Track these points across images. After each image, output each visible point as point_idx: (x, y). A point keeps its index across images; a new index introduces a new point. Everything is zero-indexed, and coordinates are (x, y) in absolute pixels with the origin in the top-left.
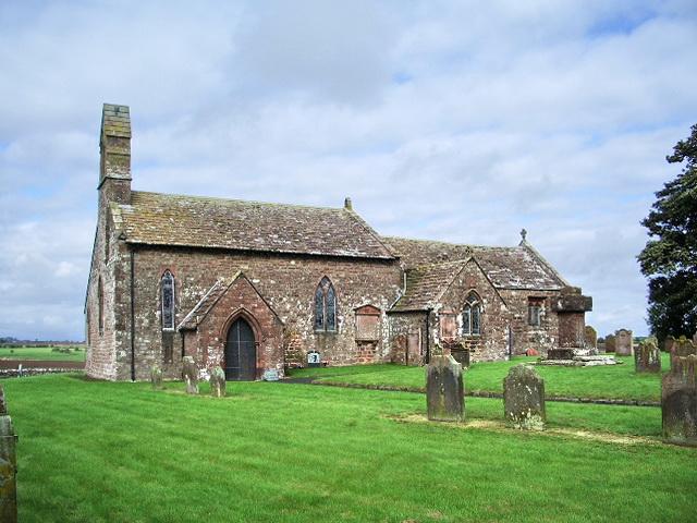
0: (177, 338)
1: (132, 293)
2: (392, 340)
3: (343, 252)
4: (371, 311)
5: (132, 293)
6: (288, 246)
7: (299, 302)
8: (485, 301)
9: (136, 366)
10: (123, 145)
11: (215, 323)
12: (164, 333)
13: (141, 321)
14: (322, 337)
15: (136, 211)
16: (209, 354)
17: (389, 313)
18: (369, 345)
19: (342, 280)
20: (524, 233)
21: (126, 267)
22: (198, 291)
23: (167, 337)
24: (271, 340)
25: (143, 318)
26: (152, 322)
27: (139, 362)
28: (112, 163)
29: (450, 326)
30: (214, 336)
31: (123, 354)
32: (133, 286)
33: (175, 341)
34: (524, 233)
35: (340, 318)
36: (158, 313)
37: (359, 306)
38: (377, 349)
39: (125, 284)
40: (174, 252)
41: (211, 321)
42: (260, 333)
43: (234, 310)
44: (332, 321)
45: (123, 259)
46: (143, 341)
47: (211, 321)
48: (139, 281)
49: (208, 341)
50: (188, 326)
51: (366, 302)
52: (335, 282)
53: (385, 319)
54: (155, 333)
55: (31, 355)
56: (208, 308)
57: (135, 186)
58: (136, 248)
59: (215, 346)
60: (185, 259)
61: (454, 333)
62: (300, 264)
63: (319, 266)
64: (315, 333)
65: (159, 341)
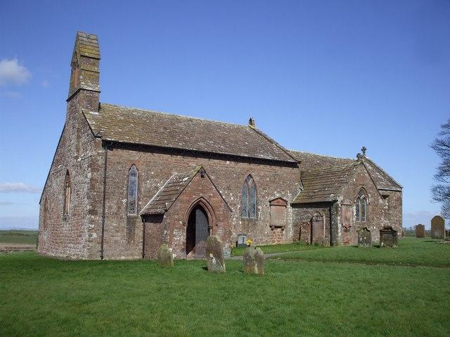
0: (139, 223)
1: (105, 183)
2: (295, 225)
3: (262, 156)
4: (280, 202)
5: (105, 183)
6: (222, 149)
7: (231, 194)
8: (370, 195)
9: (104, 246)
10: (94, 64)
11: (181, 209)
12: (129, 218)
13: (110, 207)
14: (247, 223)
15: (103, 117)
16: (174, 236)
17: (293, 205)
18: (279, 229)
19: (262, 177)
20: (364, 150)
21: (101, 161)
22: (157, 182)
23: (131, 221)
24: (222, 224)
25: (111, 204)
26: (119, 208)
27: (107, 243)
28: (84, 78)
29: (349, 214)
30: (179, 220)
31: (95, 235)
32: (105, 178)
33: (138, 225)
34: (364, 150)
35: (260, 207)
36: (124, 201)
37: (273, 198)
38: (284, 232)
39: (98, 175)
40: (139, 150)
41: (177, 208)
42: (214, 218)
43: (195, 198)
44: (255, 209)
45: (98, 153)
46: (112, 224)
47: (177, 208)
48: (109, 173)
49: (174, 224)
50: (152, 211)
51: (278, 195)
52: (257, 179)
53: (290, 209)
54: (121, 218)
55: (337, 228)
56: (169, 194)
57: (103, 99)
58: (109, 145)
59: (179, 229)
60: (147, 156)
61: (351, 220)
62: (233, 163)
63: (245, 165)
64: (242, 220)
65: (124, 224)
